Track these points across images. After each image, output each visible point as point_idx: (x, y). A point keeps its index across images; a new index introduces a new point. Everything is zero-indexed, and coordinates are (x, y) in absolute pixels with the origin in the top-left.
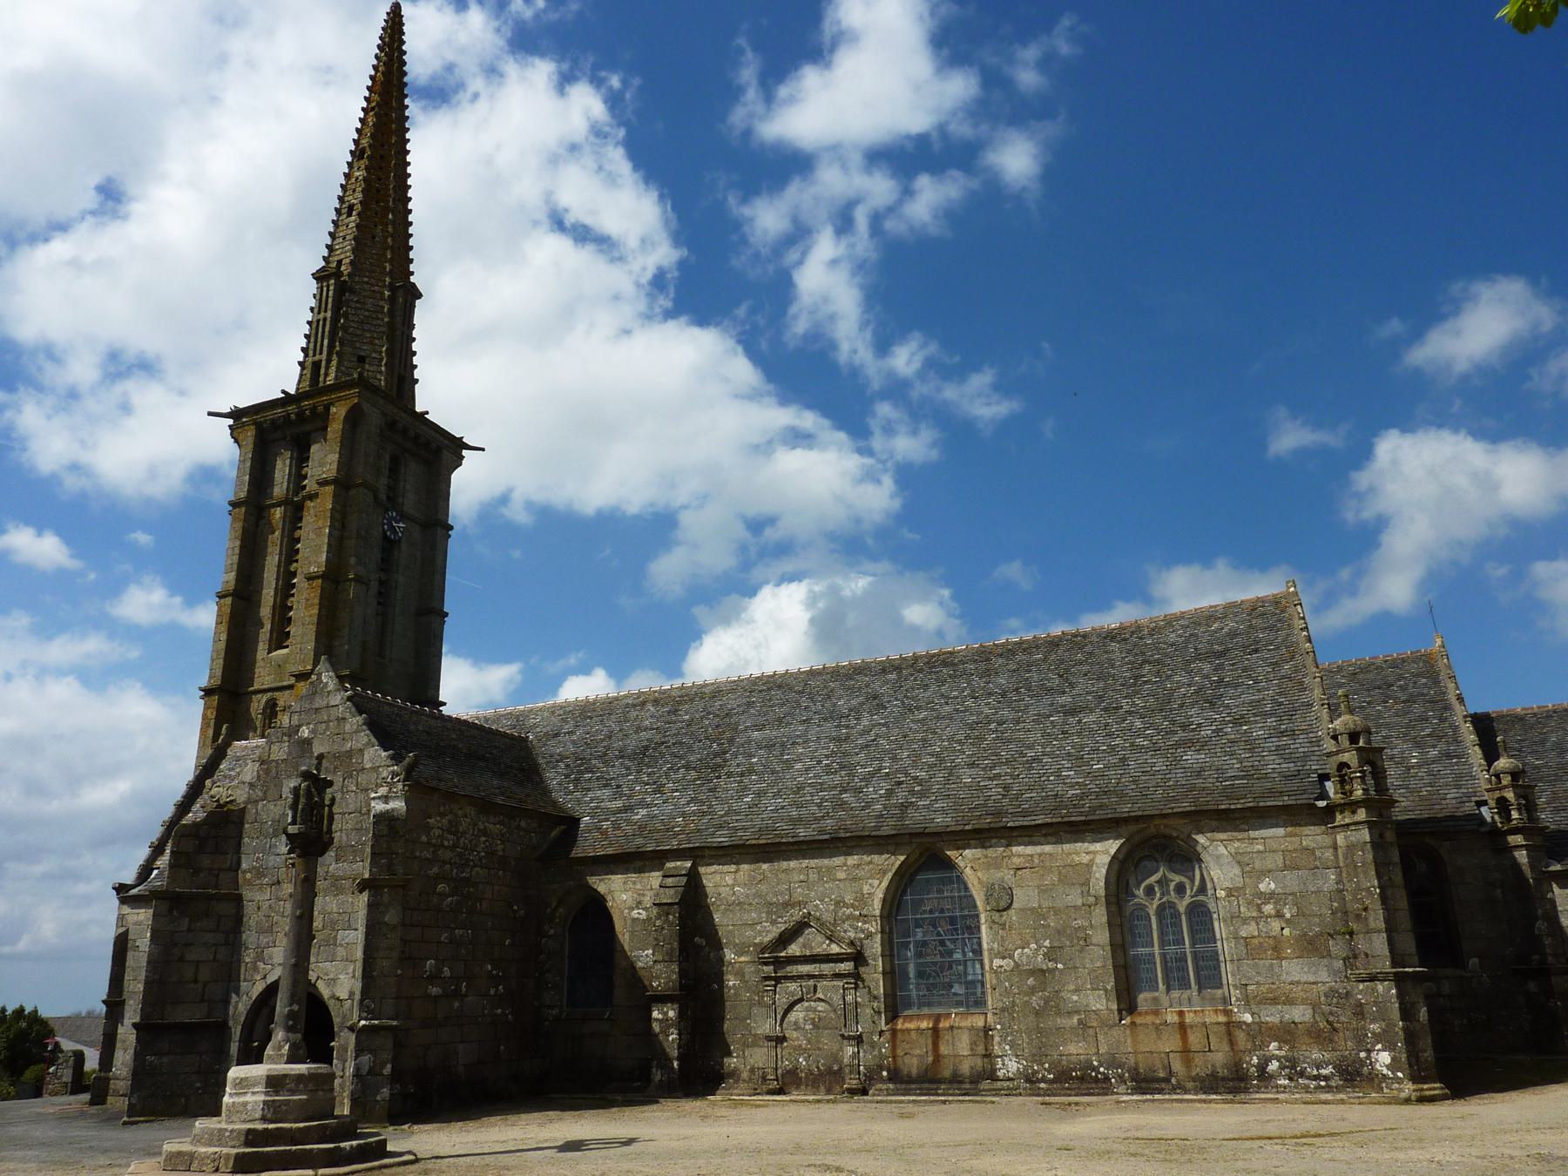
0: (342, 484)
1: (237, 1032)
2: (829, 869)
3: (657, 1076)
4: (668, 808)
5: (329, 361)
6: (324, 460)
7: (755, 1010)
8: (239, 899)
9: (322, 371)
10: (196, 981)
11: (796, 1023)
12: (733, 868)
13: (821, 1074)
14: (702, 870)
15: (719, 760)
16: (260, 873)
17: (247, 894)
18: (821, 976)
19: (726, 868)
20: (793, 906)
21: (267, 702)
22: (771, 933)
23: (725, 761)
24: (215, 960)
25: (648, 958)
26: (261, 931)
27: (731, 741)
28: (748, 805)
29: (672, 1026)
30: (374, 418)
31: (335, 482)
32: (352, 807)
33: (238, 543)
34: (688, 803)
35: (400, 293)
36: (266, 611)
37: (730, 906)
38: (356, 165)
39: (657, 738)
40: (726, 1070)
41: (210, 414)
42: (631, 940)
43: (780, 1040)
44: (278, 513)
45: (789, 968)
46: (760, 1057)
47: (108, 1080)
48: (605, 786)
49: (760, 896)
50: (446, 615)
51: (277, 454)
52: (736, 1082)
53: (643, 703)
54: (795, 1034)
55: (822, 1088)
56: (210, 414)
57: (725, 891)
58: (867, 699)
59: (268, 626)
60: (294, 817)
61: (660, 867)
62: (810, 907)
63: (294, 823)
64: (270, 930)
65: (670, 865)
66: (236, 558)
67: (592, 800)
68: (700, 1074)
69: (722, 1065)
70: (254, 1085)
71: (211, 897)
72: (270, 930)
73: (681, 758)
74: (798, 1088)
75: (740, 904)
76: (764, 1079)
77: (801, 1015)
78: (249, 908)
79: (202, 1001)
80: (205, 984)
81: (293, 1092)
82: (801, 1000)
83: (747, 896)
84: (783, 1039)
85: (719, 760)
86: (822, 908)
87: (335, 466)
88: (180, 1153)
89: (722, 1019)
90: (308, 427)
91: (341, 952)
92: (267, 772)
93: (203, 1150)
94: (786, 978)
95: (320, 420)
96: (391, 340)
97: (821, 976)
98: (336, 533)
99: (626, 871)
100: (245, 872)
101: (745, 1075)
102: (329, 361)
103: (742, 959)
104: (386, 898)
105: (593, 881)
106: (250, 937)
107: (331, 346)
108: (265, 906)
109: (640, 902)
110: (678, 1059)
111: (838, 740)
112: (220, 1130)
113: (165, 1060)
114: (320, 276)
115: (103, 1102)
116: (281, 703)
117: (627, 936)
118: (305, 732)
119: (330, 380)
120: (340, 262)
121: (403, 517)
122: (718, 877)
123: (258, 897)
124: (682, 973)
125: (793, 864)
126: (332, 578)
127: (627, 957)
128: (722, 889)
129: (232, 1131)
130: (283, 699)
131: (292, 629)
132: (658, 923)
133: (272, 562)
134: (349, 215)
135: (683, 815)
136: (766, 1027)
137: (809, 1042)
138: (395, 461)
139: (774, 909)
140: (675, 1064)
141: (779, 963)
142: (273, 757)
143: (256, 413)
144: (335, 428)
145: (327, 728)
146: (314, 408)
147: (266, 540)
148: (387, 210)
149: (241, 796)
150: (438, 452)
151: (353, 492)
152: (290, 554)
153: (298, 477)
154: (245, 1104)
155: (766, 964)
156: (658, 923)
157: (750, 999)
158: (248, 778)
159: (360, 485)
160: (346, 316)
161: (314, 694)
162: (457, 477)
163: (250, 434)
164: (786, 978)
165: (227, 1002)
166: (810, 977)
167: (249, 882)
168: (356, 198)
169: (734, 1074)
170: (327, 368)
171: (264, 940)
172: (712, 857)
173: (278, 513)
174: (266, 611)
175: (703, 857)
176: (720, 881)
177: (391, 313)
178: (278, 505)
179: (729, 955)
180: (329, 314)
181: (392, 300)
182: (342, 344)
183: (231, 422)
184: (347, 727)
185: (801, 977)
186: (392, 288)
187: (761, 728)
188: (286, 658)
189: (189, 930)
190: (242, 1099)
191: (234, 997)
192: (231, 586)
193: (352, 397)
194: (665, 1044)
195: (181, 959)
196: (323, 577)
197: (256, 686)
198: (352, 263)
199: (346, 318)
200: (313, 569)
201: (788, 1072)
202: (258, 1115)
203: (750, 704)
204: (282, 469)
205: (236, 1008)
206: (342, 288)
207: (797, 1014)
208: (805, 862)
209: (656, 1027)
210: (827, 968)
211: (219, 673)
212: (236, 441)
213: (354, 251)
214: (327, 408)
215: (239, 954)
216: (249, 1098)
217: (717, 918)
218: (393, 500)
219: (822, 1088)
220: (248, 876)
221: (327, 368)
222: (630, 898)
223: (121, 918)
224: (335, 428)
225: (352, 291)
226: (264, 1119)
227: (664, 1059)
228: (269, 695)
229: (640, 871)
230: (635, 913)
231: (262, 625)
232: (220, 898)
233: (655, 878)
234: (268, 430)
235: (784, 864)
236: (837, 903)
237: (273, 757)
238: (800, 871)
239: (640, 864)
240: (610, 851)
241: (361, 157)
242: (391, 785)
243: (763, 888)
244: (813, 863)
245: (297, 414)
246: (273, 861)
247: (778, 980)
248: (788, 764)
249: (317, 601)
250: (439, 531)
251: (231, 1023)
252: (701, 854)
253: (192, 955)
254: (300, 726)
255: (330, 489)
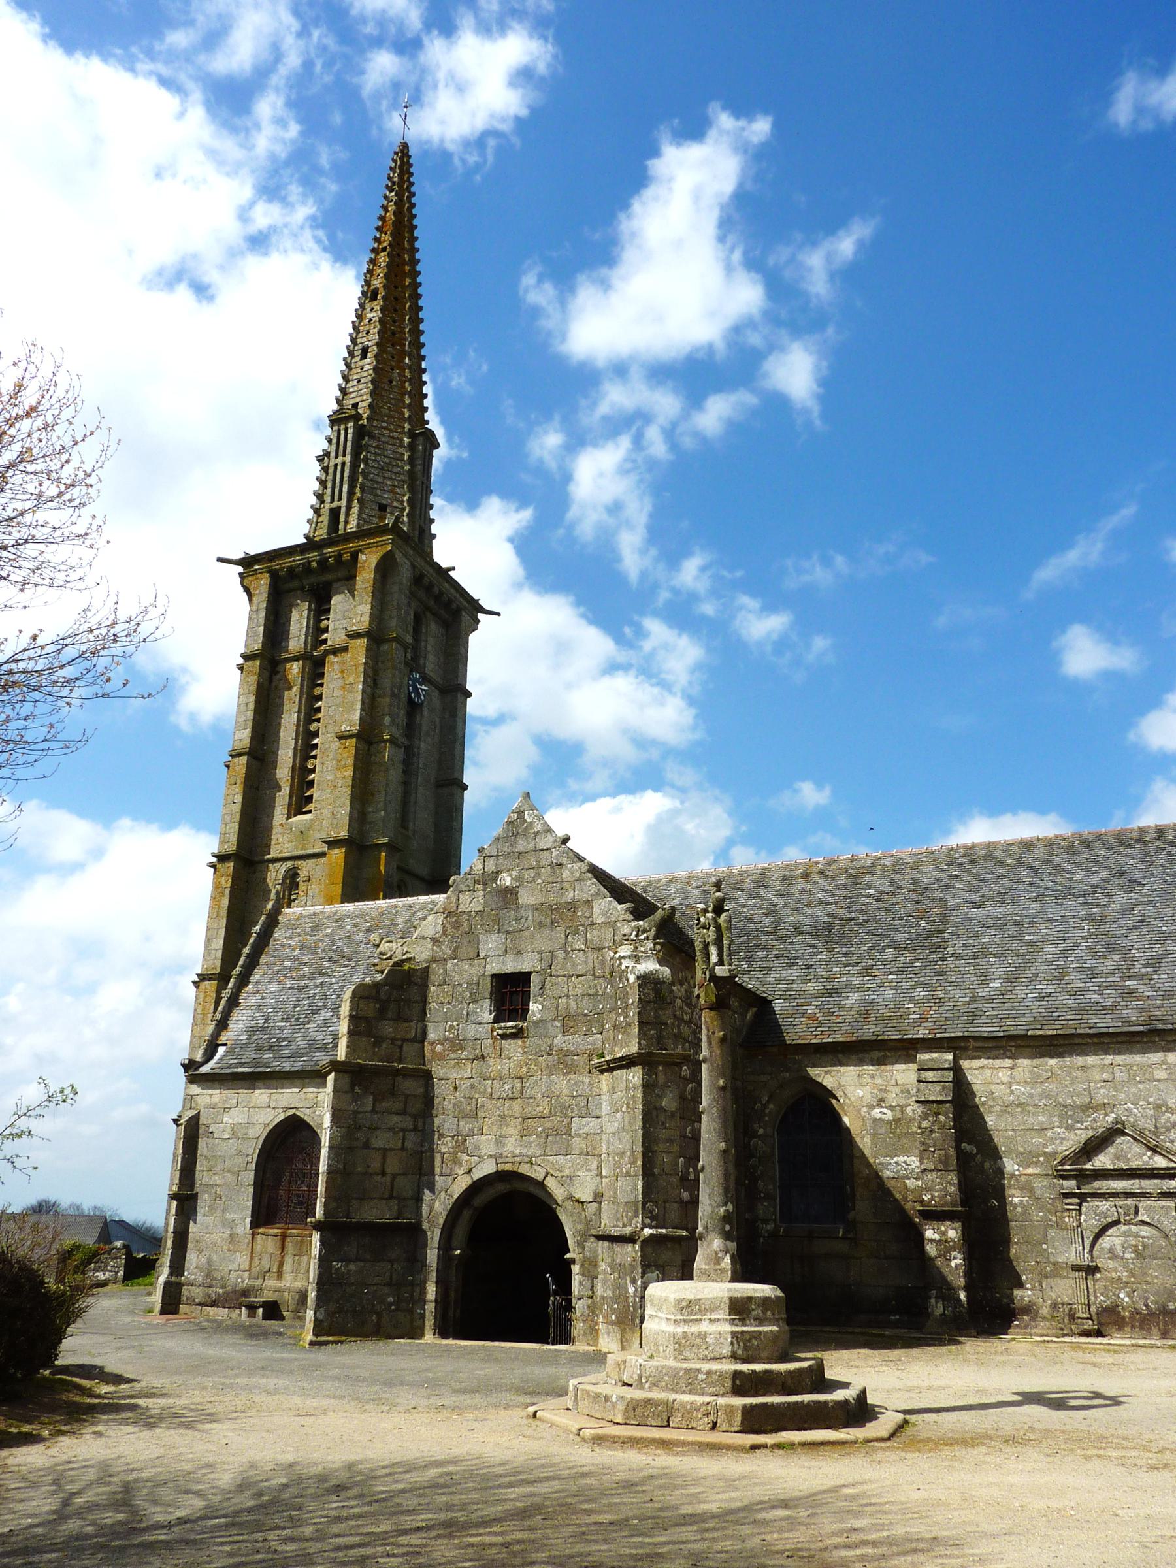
0: (375, 636)
1: (434, 1237)
2: (1141, 1067)
3: (938, 1308)
4: (886, 995)
5: (349, 508)
6: (350, 612)
7: (1052, 1233)
8: (427, 1076)
9: (342, 518)
10: (383, 1173)
11: (1111, 1251)
12: (1008, 1062)
13: (1152, 1314)
14: (965, 1064)
15: (935, 940)
16: (456, 1045)
17: (438, 1070)
18: (1143, 1195)
19: (998, 1063)
20: (1096, 1109)
21: (287, 872)
22: (1069, 1141)
23: (945, 940)
24: (403, 1148)
25: (910, 1169)
26: (461, 1116)
27: (944, 918)
28: (979, 991)
29: (954, 1248)
30: (405, 572)
31: (368, 634)
32: (580, 969)
33: (252, 698)
34: (914, 987)
35: (420, 440)
36: (283, 773)
37: (1007, 1108)
38: (368, 306)
39: (841, 914)
40: (1017, 1303)
41: (220, 560)
42: (874, 1143)
43: (1092, 1270)
44: (295, 669)
45: (1096, 1184)
46: (1066, 1289)
47: (180, 1285)
48: (791, 965)
49: (1048, 1097)
50: (465, 787)
51: (291, 606)
52: (1034, 1319)
53: (806, 875)
54: (1111, 1264)
55: (1155, 1331)
56: (220, 560)
57: (999, 1090)
58: (1113, 876)
59: (286, 790)
60: (720, 955)
61: (912, 1059)
62: (1120, 1110)
63: (721, 963)
64: (474, 1115)
65: (923, 1057)
66: (250, 715)
67: (778, 981)
68: (990, 1310)
69: (1011, 1298)
70: (711, 1310)
71: (397, 1073)
72: (474, 1115)
73: (882, 936)
74: (1121, 1328)
75: (1020, 1105)
76: (1072, 1317)
77: (1118, 1241)
78: (441, 1088)
79: (391, 1197)
80: (394, 1176)
81: (761, 1321)
82: (1117, 1222)
83: (1031, 1096)
84: (1092, 1270)
85: (935, 940)
86: (1139, 1116)
87: (366, 618)
88: (648, 1402)
89: (1006, 1242)
90: (329, 577)
91: (578, 1144)
92: (457, 926)
93: (687, 1398)
94: (1094, 1195)
95: (346, 572)
96: (412, 489)
97: (1143, 1195)
98: (369, 690)
99: (861, 1062)
100: (433, 1043)
101: (1045, 1311)
102: (349, 508)
103: (1030, 1171)
104: (661, 1079)
105: (815, 1072)
106: (445, 1122)
107: (351, 493)
108: (464, 1086)
109: (882, 1100)
110: (966, 1288)
111: (1090, 918)
112: (688, 1371)
113: (352, 1267)
114: (334, 421)
115: (175, 1311)
116: (303, 873)
117: (867, 1139)
118: (506, 880)
119: (353, 526)
120: (355, 406)
121: (425, 679)
122: (988, 1073)
123: (454, 1074)
124: (963, 1186)
125: (1091, 1060)
126: (366, 738)
127: (869, 1165)
128: (993, 1087)
129: (709, 1373)
130: (306, 868)
131: (315, 792)
132: (925, 1124)
133: (289, 720)
134: (364, 356)
135: (912, 1000)
136: (1074, 1253)
137: (1132, 1273)
138: (418, 620)
139: (1070, 1113)
140: (963, 1295)
141: (1083, 1177)
142: (462, 908)
143: (271, 561)
144: (365, 577)
145: (538, 875)
146: (340, 555)
147: (281, 697)
148: (403, 354)
149: (421, 953)
150: (456, 613)
151: (385, 647)
152: (310, 711)
153: (317, 632)
154: (703, 1336)
155: (1064, 1177)
156: (925, 1124)
157: (1045, 1220)
158: (430, 933)
159: (394, 639)
160: (366, 460)
161: (515, 835)
162: (473, 638)
163: (262, 584)
164: (1094, 1195)
165: (419, 1199)
166: (1128, 1195)
167: (441, 1057)
168: (371, 339)
169: (1027, 1310)
170: (347, 514)
171: (466, 1126)
172: (976, 1049)
173: (295, 668)
174: (283, 773)
175: (966, 1049)
176: (990, 1078)
177: (411, 461)
178: (296, 659)
179: (1010, 1165)
180: (348, 459)
181: (412, 447)
182: (362, 491)
183: (240, 569)
184: (566, 875)
185: (1115, 1195)
186: (412, 435)
187: (979, 905)
188: (310, 825)
189: (374, 1111)
190: (695, 1328)
191: (427, 1195)
192: (246, 744)
193: (386, 544)
194: (946, 1271)
195: (367, 1146)
196: (358, 736)
197: (274, 854)
198: (370, 406)
199: (366, 464)
200: (345, 728)
201: (1105, 1310)
202: (726, 1350)
203: (952, 879)
204: (299, 620)
205: (431, 1208)
206: (360, 432)
207: (1112, 1239)
208: (1109, 1059)
209: (932, 1250)
210: (1149, 1185)
211: (233, 837)
212: (247, 590)
213: (373, 393)
214: (355, 556)
215: (432, 1142)
216: (705, 1327)
217: (990, 1121)
218: (414, 663)
219: (1155, 1331)
220: (439, 1048)
221: (347, 514)
222: (870, 1100)
223: (189, 1100)
224: (365, 577)
225: (372, 436)
226: (734, 1357)
227: (946, 1291)
228: (290, 864)
229: (880, 1062)
230: (876, 1113)
231: (279, 788)
232: (405, 1074)
233: (904, 1074)
234: (287, 582)
235: (1079, 1060)
236: (1158, 1107)
237: (462, 908)
238: (1103, 1068)
239: (877, 1054)
240: (838, 1038)
241: (374, 297)
242: (635, 944)
243: (1052, 1087)
244: (1119, 1059)
245: (319, 562)
246: (472, 1031)
247: (1083, 1198)
248: (1035, 947)
249: (351, 761)
250: (460, 697)
251: (425, 1226)
252: (961, 1046)
253: (378, 1142)
254: (498, 873)
255: (362, 642)
